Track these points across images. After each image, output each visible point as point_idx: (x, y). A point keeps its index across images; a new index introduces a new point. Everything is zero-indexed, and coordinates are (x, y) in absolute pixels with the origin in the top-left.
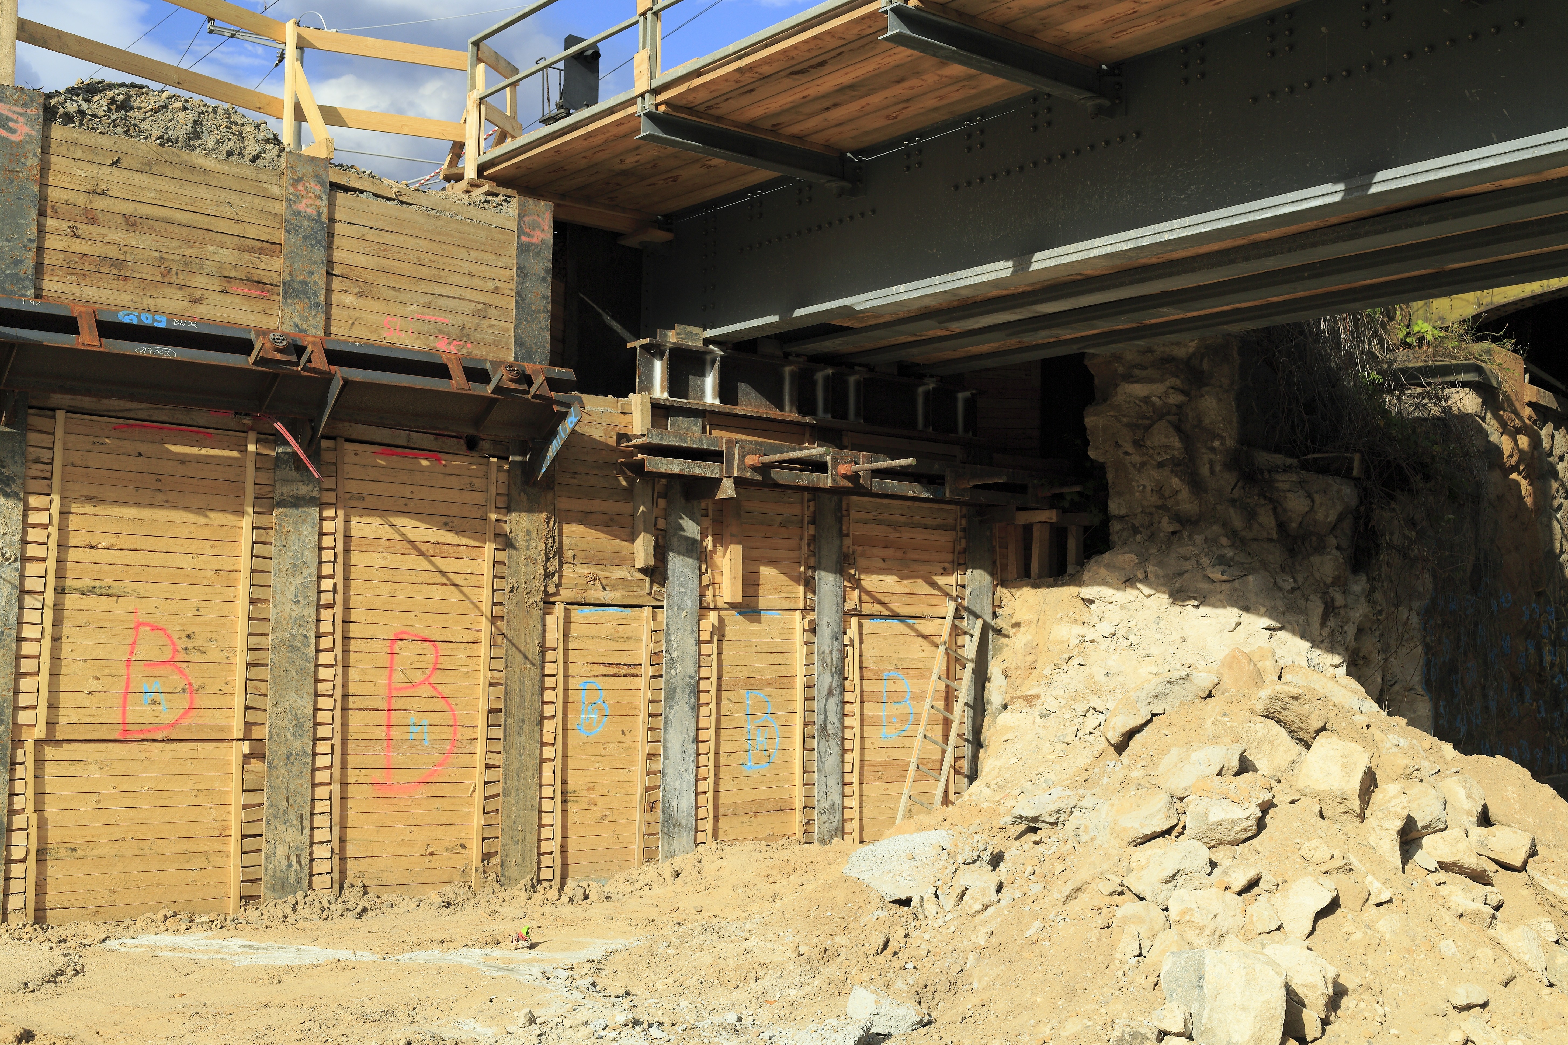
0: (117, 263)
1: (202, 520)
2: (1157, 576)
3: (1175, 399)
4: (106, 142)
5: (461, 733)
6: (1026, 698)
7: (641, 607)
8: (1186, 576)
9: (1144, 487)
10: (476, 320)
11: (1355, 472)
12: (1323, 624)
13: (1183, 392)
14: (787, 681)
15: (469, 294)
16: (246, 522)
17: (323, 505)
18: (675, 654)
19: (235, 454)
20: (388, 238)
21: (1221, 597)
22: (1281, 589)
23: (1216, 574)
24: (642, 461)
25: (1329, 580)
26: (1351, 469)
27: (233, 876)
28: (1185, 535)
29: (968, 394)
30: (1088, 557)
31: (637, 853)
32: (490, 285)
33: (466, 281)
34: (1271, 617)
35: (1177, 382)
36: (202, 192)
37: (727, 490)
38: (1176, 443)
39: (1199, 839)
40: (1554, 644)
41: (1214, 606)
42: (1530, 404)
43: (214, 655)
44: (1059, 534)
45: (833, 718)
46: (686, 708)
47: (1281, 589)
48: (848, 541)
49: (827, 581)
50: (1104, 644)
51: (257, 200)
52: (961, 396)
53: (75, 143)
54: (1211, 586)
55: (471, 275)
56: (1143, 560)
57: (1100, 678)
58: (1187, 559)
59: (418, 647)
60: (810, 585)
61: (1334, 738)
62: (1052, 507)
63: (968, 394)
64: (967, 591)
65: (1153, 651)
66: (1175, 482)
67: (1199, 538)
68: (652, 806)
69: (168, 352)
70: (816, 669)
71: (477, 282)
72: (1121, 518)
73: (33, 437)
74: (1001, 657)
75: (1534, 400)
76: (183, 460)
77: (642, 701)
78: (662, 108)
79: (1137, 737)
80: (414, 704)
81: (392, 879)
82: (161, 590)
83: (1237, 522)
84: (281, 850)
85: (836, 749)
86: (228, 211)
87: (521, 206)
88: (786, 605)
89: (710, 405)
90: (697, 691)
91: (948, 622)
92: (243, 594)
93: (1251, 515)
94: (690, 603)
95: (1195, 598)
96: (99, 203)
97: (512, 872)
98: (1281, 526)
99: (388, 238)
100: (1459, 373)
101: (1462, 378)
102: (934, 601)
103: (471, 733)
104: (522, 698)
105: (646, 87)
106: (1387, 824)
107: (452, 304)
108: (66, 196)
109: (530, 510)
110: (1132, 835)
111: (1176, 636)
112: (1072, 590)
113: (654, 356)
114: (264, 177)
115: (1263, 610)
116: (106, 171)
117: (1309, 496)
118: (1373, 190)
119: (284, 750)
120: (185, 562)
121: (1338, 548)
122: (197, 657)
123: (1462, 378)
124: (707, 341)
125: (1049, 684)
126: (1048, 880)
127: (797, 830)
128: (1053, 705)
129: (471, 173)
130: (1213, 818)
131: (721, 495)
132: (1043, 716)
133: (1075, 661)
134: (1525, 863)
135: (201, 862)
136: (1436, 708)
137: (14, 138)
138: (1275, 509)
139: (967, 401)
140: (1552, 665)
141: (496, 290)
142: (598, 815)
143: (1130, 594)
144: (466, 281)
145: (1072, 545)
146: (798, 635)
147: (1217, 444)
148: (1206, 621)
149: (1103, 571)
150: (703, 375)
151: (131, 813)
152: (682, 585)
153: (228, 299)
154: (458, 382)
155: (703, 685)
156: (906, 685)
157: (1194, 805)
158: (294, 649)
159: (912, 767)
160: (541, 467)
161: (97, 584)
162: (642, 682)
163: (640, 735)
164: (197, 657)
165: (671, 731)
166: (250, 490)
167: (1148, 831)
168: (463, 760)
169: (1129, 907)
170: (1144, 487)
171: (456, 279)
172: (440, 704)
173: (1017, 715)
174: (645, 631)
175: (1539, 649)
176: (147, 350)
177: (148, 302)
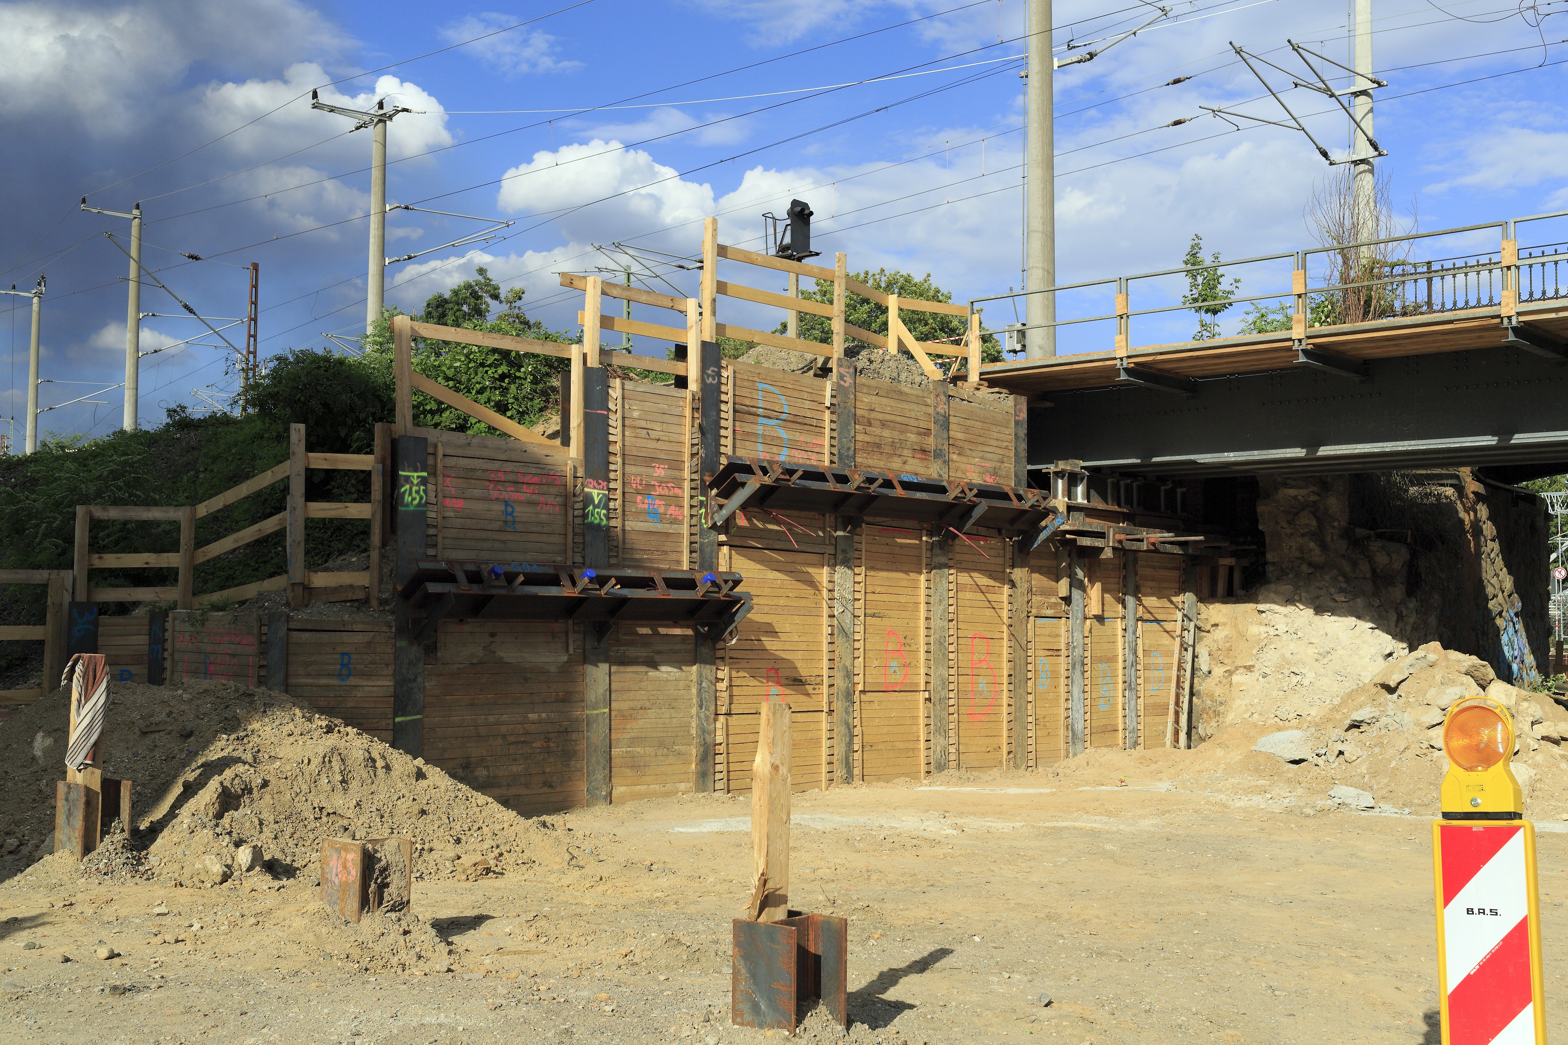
0: (879, 446)
1: (907, 577)
2: (1306, 599)
3: (1313, 498)
7: (1060, 618)
8: (1321, 598)
9: (1291, 547)
10: (999, 464)
11: (1409, 540)
12: (1396, 626)
13: (1318, 495)
14: (1113, 659)
16: (923, 578)
17: (950, 567)
18: (1075, 644)
19: (917, 542)
20: (969, 423)
21: (1343, 610)
22: (1373, 606)
23: (1341, 598)
25: (1398, 601)
26: (1406, 539)
27: (923, 760)
28: (1318, 575)
29: (1184, 489)
32: (1005, 444)
33: (995, 443)
34: (1373, 622)
35: (1315, 489)
36: (905, 406)
37: (1108, 554)
38: (1314, 523)
41: (1339, 615)
42: (1473, 493)
45: (1133, 679)
47: (1373, 606)
48: (1138, 578)
49: (1130, 600)
54: (1336, 604)
55: (997, 440)
56: (1297, 588)
57: (1288, 656)
58: (1320, 589)
60: (1123, 603)
62: (1232, 557)
63: (1184, 489)
64: (1186, 606)
66: (1312, 545)
67: (1327, 577)
71: (999, 443)
72: (1274, 564)
75: (1476, 490)
76: (902, 546)
78: (1132, 365)
80: (982, 672)
82: (894, 613)
83: (1347, 568)
84: (939, 748)
86: (913, 415)
87: (1015, 400)
89: (1080, 504)
91: (1179, 623)
92: (922, 614)
93: (1355, 564)
94: (1080, 615)
95: (1329, 611)
96: (873, 415)
97: (1019, 762)
98: (1374, 571)
99: (969, 423)
100: (1448, 479)
101: (1449, 482)
102: (1172, 611)
104: (1020, 668)
106: (1527, 719)
109: (1021, 567)
110: (1427, 725)
112: (1251, 606)
113: (1058, 477)
115: (1368, 618)
116: (874, 398)
117: (1389, 555)
118: (1512, 442)
122: (908, 648)
123: (1449, 482)
124: (1082, 468)
131: (1103, 556)
138: (1370, 562)
139: (1183, 494)
141: (1006, 448)
143: (1290, 609)
144: (995, 443)
146: (1120, 632)
147: (1336, 524)
148: (1337, 624)
149: (1272, 595)
150: (1076, 486)
152: (1077, 606)
156: (1161, 660)
160: (1033, 544)
161: (876, 611)
162: (1062, 659)
163: (1063, 689)
164: (908, 648)
166: (924, 561)
167: (1435, 723)
170: (1291, 547)
171: (992, 442)
174: (1063, 630)
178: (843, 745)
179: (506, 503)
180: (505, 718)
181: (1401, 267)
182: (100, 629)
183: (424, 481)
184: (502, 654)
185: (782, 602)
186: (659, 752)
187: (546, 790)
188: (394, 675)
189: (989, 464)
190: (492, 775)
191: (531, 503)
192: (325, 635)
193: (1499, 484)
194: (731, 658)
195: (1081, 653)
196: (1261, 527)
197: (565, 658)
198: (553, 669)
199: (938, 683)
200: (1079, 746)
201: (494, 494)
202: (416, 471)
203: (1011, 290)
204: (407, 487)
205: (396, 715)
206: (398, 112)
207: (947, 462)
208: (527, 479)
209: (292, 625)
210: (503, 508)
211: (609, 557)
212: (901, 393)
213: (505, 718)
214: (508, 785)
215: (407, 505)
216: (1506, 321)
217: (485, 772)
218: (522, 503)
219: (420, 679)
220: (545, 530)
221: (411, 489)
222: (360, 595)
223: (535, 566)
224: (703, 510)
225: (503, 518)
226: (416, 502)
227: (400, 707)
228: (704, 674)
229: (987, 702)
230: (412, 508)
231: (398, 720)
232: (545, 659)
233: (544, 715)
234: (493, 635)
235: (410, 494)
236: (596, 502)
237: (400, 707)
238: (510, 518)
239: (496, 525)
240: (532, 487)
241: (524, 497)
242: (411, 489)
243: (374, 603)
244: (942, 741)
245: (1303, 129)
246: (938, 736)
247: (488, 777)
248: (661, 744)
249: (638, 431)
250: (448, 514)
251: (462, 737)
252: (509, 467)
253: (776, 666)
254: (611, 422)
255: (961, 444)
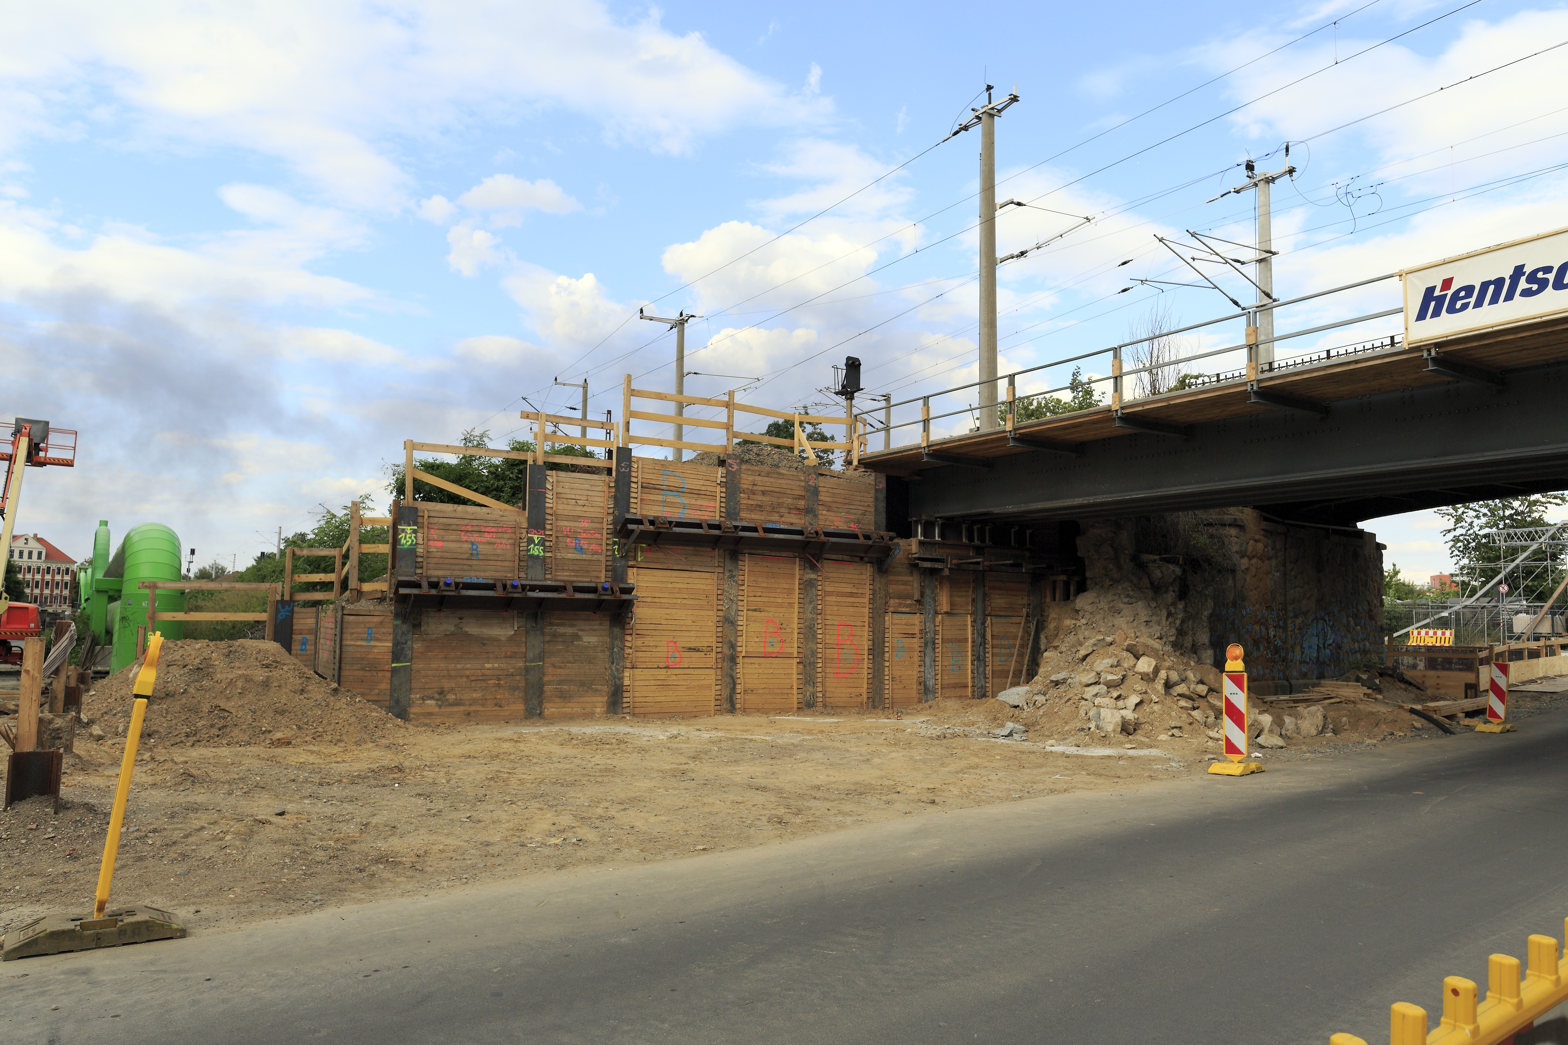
0: (760, 506)
4: (756, 468)
5: (860, 657)
6: (1054, 647)
12: (1167, 619)
14: (966, 640)
15: (860, 508)
20: (835, 491)
22: (1151, 607)
24: (918, 564)
25: (1169, 604)
29: (1031, 531)
30: (1078, 593)
31: (916, 700)
32: (866, 504)
33: (859, 503)
36: (782, 481)
37: (946, 572)
39: (1104, 684)
40: (1275, 627)
43: (788, 630)
44: (1067, 584)
45: (982, 654)
46: (931, 649)
47: (1151, 607)
50: (1083, 627)
51: (798, 482)
52: (1028, 532)
53: (749, 470)
55: (860, 501)
57: (1082, 639)
58: (1115, 595)
59: (846, 628)
61: (1146, 657)
63: (1031, 531)
65: (1102, 630)
66: (1111, 566)
67: (1120, 587)
68: (920, 684)
69: (782, 536)
70: (976, 636)
71: (862, 503)
73: (740, 563)
74: (1044, 632)
77: (916, 646)
79: (1089, 657)
81: (840, 704)
82: (773, 609)
84: (808, 693)
85: (983, 665)
86: (789, 487)
88: (965, 612)
90: (934, 643)
96: (755, 488)
97: (876, 704)
98: (1152, 583)
99: (835, 491)
103: (863, 657)
105: (926, 445)
107: (855, 511)
108: (746, 486)
110: (1085, 684)
111: (1110, 624)
114: (799, 474)
119: (808, 661)
120: (780, 600)
121: (1174, 591)
122: (784, 631)
125: (1063, 642)
126: (1060, 698)
127: (970, 694)
128: (1064, 649)
129: (855, 463)
130: (1108, 679)
132: (1061, 653)
133: (1073, 633)
134: (1207, 695)
135: (786, 696)
136: (1215, 652)
137: (733, 470)
140: (1274, 636)
141: (868, 506)
142: (903, 686)
144: (859, 503)
145: (1072, 588)
147: (1127, 552)
151: (767, 680)
153: (790, 515)
154: (862, 540)
155: (937, 641)
157: (1103, 675)
158: (811, 628)
159: (1011, 673)
165: (927, 658)
168: (860, 666)
169: (1083, 702)
172: (853, 647)
173: (1051, 653)
175: (1267, 629)
176: (776, 536)
177: (769, 518)
178: (728, 689)
179: (473, 543)
180: (468, 666)
181: (1202, 378)
182: (295, 615)
183: (415, 532)
184: (467, 629)
185: (679, 601)
186: (581, 689)
187: (497, 708)
188: (393, 640)
189: (852, 517)
190: (458, 698)
191: (490, 543)
192: (361, 618)
193: (1307, 524)
194: (637, 634)
195: (933, 636)
196: (1079, 554)
197: (513, 633)
198: (503, 638)
199: (809, 653)
200: (930, 696)
201: (464, 538)
202: (409, 525)
203: (970, 405)
204: (403, 535)
205: (393, 662)
206: (689, 317)
207: (816, 516)
208: (487, 529)
209: (345, 612)
210: (470, 546)
211: (545, 574)
212: (779, 474)
213: (468, 666)
214: (470, 705)
215: (403, 545)
216: (1114, 414)
217: (454, 697)
218: (484, 543)
219: (409, 643)
220: (500, 558)
221: (406, 536)
222: (379, 595)
223: (481, 579)
224: (617, 547)
225: (470, 552)
226: (409, 543)
227: (396, 658)
228: (615, 644)
229: (850, 666)
230: (406, 547)
231: (394, 665)
232: (497, 633)
233: (496, 665)
234: (461, 618)
235: (405, 538)
236: (536, 542)
237: (396, 658)
238: (474, 552)
239: (466, 556)
240: (491, 534)
241: (485, 540)
242: (406, 536)
243: (388, 600)
244: (811, 689)
245: (1216, 287)
246: (808, 686)
247: (456, 699)
248: (582, 684)
249: (569, 500)
250: (431, 550)
251: (438, 676)
252: (475, 523)
253: (674, 640)
254: (547, 495)
255: (830, 504)
